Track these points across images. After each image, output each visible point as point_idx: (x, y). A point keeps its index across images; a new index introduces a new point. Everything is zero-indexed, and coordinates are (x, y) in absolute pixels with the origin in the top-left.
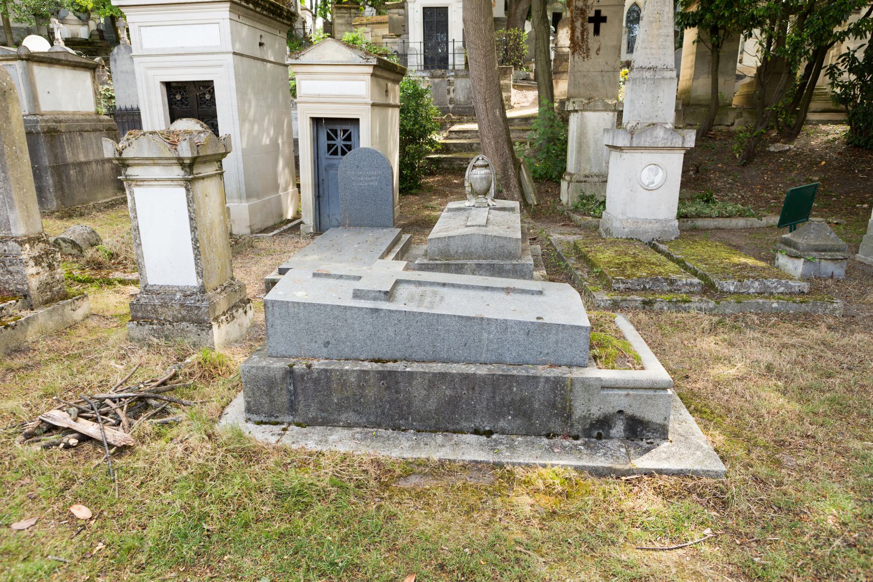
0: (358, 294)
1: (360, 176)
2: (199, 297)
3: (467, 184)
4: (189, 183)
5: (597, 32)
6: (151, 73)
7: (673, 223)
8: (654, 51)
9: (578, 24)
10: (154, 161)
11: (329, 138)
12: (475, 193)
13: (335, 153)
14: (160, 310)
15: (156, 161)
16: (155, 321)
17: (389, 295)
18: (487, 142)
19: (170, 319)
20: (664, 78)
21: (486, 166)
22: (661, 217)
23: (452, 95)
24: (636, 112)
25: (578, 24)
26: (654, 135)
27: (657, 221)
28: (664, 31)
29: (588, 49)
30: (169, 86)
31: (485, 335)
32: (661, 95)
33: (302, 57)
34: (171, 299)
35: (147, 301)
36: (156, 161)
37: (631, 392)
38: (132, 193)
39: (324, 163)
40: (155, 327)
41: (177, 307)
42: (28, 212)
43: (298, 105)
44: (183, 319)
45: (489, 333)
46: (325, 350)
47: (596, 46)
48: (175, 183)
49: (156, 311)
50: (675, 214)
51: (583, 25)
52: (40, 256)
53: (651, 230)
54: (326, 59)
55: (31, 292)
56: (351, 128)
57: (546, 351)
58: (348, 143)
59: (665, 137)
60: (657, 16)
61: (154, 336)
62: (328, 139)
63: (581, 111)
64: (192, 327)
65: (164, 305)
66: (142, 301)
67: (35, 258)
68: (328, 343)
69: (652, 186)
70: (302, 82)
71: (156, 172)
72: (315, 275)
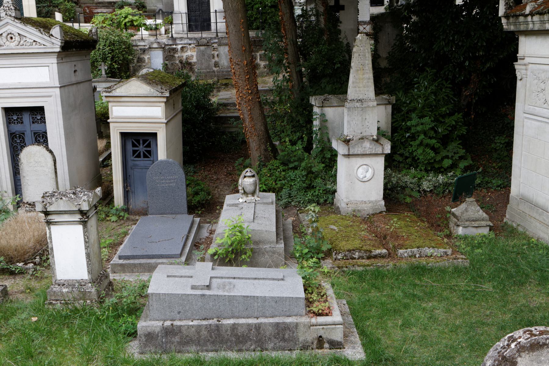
0: (193, 287)
3: (240, 188)
4: (84, 223)
7: (381, 203)
8: (361, 89)
11: (134, 145)
12: (245, 193)
13: (139, 156)
17: (208, 287)
20: (368, 107)
21: (253, 176)
22: (373, 199)
23: (216, 59)
24: (351, 129)
26: (364, 146)
27: (370, 202)
28: (367, 76)
32: (367, 117)
37: (324, 327)
39: (130, 163)
43: (111, 124)
45: (258, 303)
46: (179, 315)
50: (382, 196)
53: (367, 209)
56: (151, 140)
58: (148, 149)
59: (371, 147)
60: (361, 66)
62: (140, 157)
68: (180, 312)
69: (365, 179)
70: (114, 108)
72: (168, 276)
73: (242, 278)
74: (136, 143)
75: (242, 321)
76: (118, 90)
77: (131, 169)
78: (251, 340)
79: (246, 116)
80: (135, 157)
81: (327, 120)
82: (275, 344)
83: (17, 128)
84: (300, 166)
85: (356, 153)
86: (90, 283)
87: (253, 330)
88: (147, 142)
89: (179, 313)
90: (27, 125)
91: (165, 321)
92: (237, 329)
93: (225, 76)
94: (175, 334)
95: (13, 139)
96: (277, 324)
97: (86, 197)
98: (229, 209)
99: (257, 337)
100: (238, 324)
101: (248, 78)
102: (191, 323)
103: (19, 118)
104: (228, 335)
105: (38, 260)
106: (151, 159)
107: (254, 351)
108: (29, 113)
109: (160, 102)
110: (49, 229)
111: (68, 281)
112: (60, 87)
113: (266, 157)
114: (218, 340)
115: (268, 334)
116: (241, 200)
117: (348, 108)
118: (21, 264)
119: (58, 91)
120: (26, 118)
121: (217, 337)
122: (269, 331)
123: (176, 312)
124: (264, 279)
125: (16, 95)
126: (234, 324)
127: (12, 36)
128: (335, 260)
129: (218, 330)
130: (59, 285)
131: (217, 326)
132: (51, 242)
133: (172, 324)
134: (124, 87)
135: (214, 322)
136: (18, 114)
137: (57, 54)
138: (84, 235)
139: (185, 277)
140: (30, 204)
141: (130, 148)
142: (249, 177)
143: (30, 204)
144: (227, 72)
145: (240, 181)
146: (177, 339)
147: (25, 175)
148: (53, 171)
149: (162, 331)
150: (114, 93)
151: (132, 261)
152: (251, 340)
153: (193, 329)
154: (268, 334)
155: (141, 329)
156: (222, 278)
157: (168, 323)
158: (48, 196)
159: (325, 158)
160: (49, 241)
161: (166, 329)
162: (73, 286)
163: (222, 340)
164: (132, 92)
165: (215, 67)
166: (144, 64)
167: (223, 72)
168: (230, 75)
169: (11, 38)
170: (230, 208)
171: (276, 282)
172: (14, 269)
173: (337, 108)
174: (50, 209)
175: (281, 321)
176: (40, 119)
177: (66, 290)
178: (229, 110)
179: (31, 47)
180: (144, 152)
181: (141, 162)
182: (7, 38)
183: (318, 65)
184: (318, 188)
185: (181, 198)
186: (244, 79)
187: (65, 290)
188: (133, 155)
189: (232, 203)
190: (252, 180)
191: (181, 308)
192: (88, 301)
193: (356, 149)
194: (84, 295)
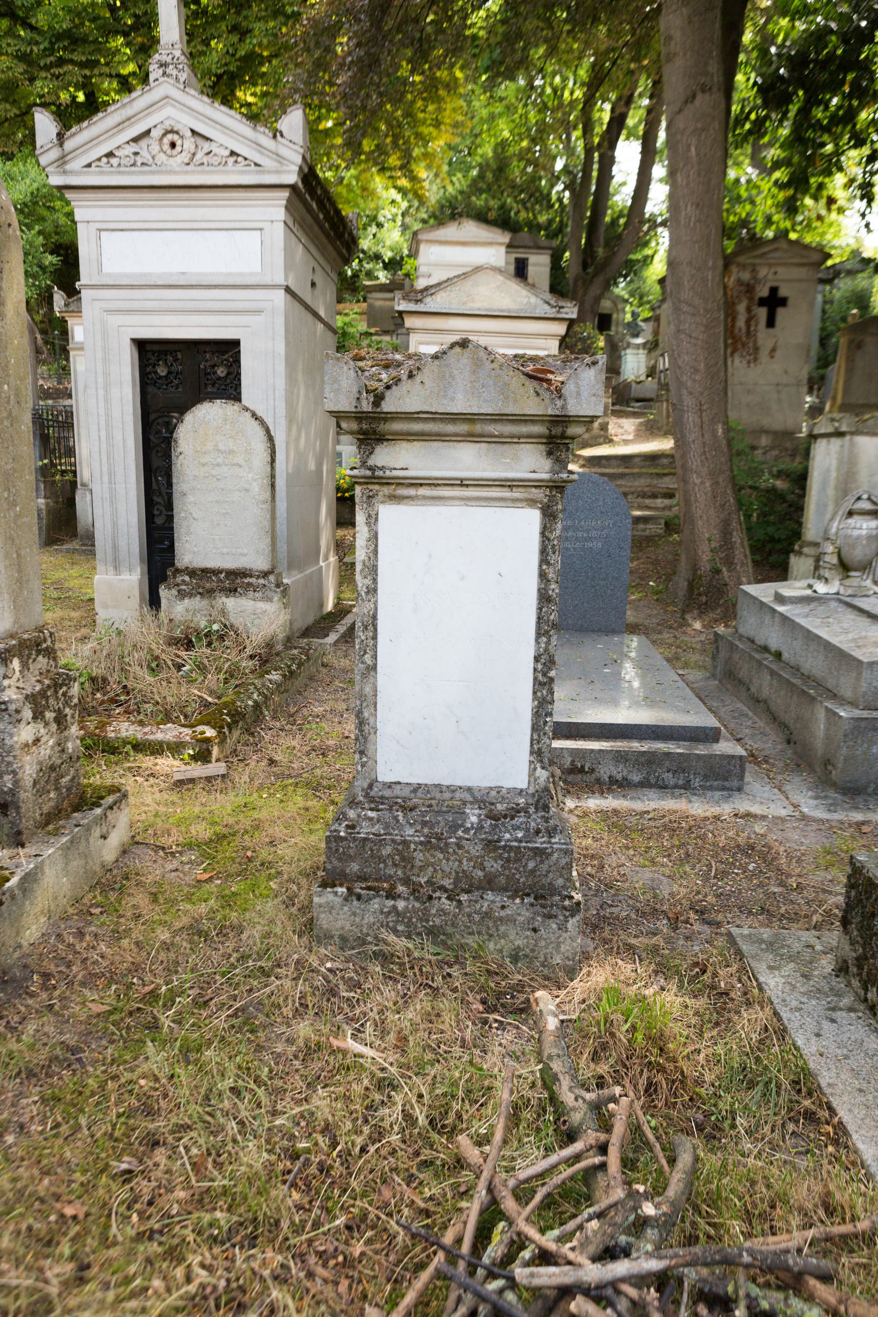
2: (535, 820)
5: (771, 323)
9: (741, 308)
10: (470, 427)
14: (419, 856)
15: (478, 428)
16: (401, 888)
18: (698, 481)
19: (447, 883)
25: (741, 308)
29: (757, 349)
30: (143, 346)
33: (428, 300)
34: (454, 827)
35: (378, 828)
36: (478, 428)
38: (373, 520)
40: (401, 905)
41: (475, 850)
42: (20, 571)
44: (489, 883)
47: (769, 344)
48: (517, 494)
49: (407, 860)
51: (749, 310)
52: (43, 693)
54: (477, 305)
55: (23, 795)
61: (395, 931)
63: (852, 433)
64: (519, 909)
65: (434, 843)
66: (365, 830)
67: (31, 698)
71: (467, 460)
127: (175, 137)
132: (373, 591)
137: (286, 194)
148: (267, 481)
169: (173, 145)
179: (221, 168)
182: (164, 135)
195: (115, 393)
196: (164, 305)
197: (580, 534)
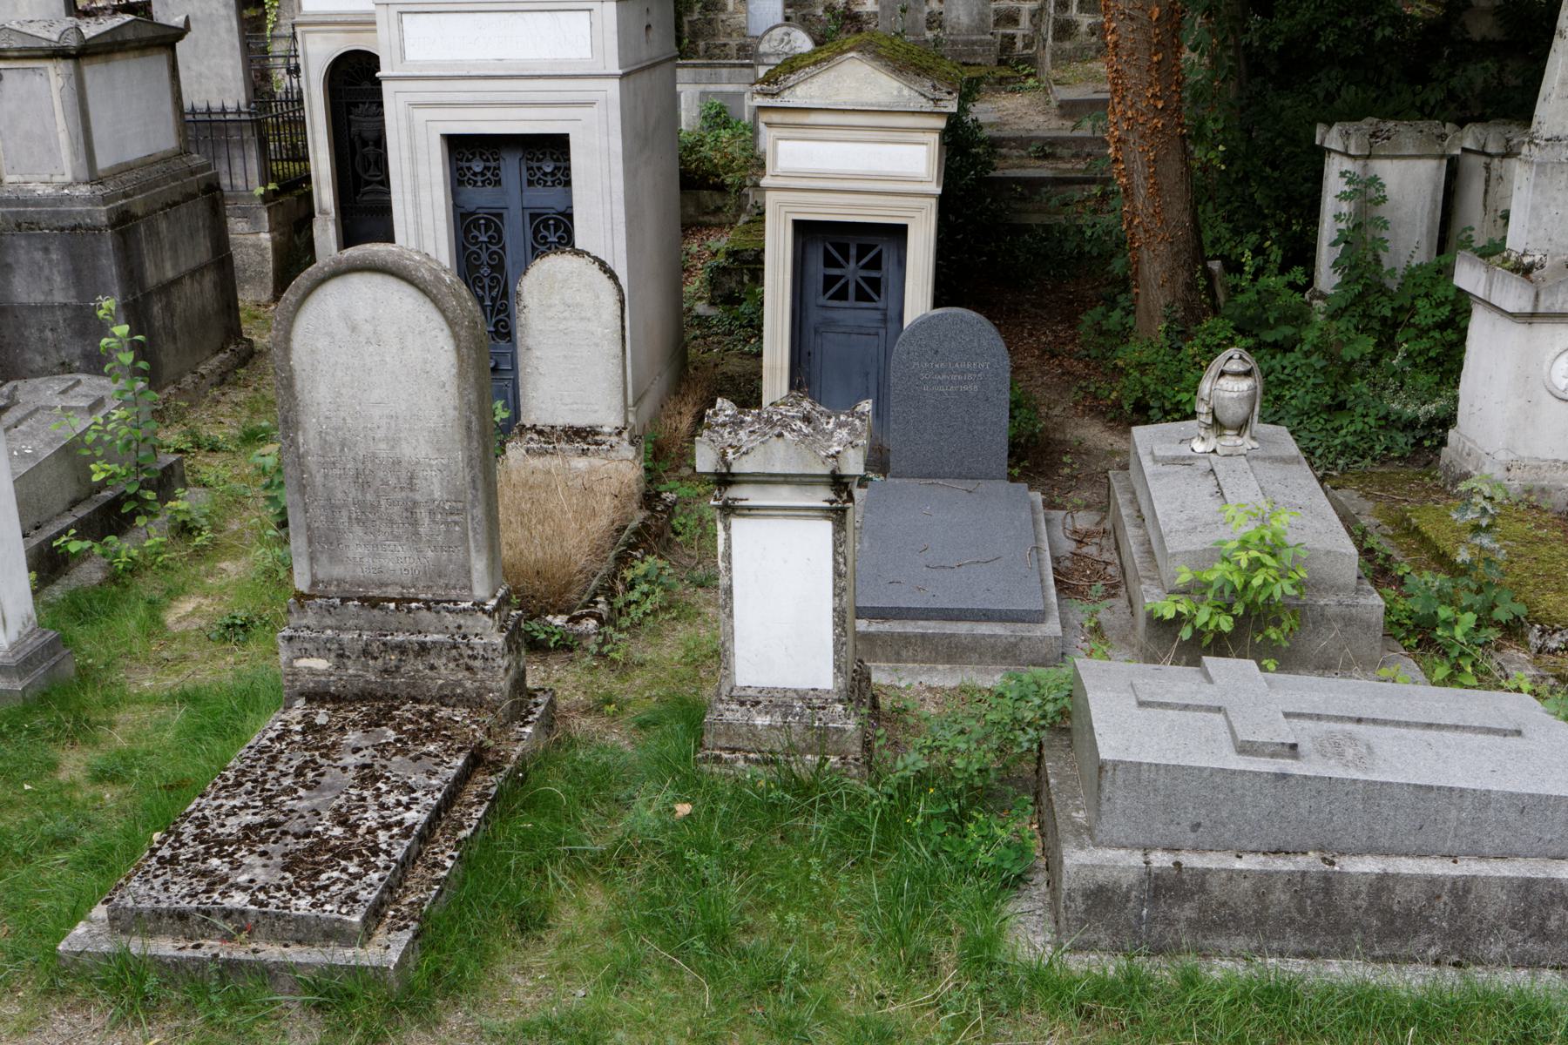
1: (940, 372)
4: (837, 515)
6: (421, 115)
11: (829, 261)
12: (1218, 425)
13: (842, 295)
21: (1248, 374)
24: (1541, 233)
31: (1454, 812)
39: (814, 316)
46: (1193, 835)
57: (1549, 837)
58: (874, 274)
68: (1199, 825)
70: (782, 145)
72: (1142, 704)
73: (1385, 723)
74: (836, 254)
75: (1406, 866)
76: (800, 90)
77: (816, 332)
78: (1430, 928)
79: (1138, 179)
80: (832, 298)
81: (1384, 199)
82: (1510, 946)
83: (481, 197)
84: (1302, 340)
85: (1557, 309)
86: (840, 701)
87: (1445, 898)
88: (871, 254)
89: (1196, 827)
90: (513, 193)
91: (1146, 850)
92: (1392, 891)
93: (960, 55)
94: (1186, 896)
95: (467, 231)
96: (1528, 885)
97: (845, 432)
98: (1167, 474)
99: (1452, 918)
100: (1396, 877)
101: (1158, 63)
102: (1239, 865)
103: (488, 168)
104: (1357, 909)
105: (602, 607)
106: (880, 305)
107: (1437, 963)
108: (519, 155)
109: (924, 130)
110: (727, 528)
111: (770, 691)
112: (622, 77)
113: (1189, 309)
114: (1322, 922)
115: (1491, 912)
116: (1199, 447)
117: (1539, 165)
118: (560, 620)
119: (613, 87)
120: (512, 167)
121: (1323, 915)
122: (1496, 904)
123: (1186, 825)
124: (1457, 727)
125: (489, 98)
126: (1383, 877)
128: (1540, 651)
129: (1327, 892)
130: (742, 704)
131: (1327, 878)
132: (729, 570)
133: (1178, 864)
134: (819, 81)
135: (1310, 862)
136: (487, 155)
138: (835, 552)
139: (1198, 708)
140: (540, 433)
141: (817, 269)
142: (1236, 374)
143: (540, 433)
144: (966, 43)
145: (1205, 387)
146: (1188, 911)
147: (530, 342)
148: (618, 336)
149: (1142, 882)
150: (788, 99)
151: (895, 627)
152: (1430, 928)
153: (1246, 884)
154: (1491, 912)
155: (1077, 873)
156: (1319, 717)
157: (1161, 860)
158: (724, 425)
159: (1371, 317)
160: (721, 565)
161: (1157, 877)
162: (786, 709)
163: (1337, 923)
164: (844, 98)
165: (930, 29)
166: (723, 16)
167: (954, 43)
168: (974, 53)
170: (1167, 469)
171: (1498, 739)
172: (543, 636)
173: (1411, 162)
174: (742, 466)
175: (1541, 875)
176: (552, 174)
177: (767, 720)
178: (1005, 157)
180: (857, 284)
181: (851, 314)
183: (1323, 28)
184: (1359, 410)
185: (997, 431)
186: (1145, 64)
187: (761, 721)
188: (825, 292)
189: (1170, 453)
190: (1244, 385)
191: (1203, 812)
192: (833, 759)
193: (1560, 298)
194: (823, 739)
195: (425, 196)
196: (479, 97)
197: (954, 377)
